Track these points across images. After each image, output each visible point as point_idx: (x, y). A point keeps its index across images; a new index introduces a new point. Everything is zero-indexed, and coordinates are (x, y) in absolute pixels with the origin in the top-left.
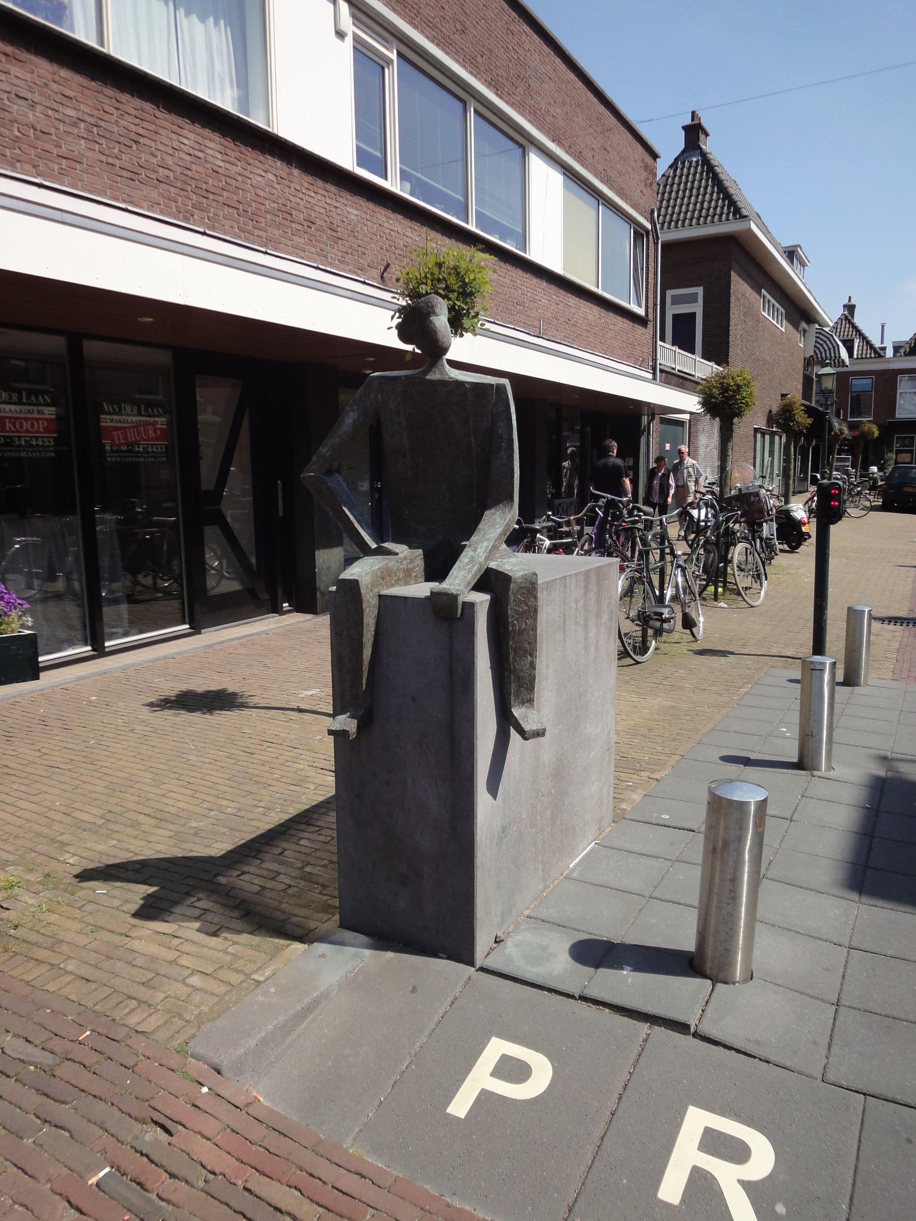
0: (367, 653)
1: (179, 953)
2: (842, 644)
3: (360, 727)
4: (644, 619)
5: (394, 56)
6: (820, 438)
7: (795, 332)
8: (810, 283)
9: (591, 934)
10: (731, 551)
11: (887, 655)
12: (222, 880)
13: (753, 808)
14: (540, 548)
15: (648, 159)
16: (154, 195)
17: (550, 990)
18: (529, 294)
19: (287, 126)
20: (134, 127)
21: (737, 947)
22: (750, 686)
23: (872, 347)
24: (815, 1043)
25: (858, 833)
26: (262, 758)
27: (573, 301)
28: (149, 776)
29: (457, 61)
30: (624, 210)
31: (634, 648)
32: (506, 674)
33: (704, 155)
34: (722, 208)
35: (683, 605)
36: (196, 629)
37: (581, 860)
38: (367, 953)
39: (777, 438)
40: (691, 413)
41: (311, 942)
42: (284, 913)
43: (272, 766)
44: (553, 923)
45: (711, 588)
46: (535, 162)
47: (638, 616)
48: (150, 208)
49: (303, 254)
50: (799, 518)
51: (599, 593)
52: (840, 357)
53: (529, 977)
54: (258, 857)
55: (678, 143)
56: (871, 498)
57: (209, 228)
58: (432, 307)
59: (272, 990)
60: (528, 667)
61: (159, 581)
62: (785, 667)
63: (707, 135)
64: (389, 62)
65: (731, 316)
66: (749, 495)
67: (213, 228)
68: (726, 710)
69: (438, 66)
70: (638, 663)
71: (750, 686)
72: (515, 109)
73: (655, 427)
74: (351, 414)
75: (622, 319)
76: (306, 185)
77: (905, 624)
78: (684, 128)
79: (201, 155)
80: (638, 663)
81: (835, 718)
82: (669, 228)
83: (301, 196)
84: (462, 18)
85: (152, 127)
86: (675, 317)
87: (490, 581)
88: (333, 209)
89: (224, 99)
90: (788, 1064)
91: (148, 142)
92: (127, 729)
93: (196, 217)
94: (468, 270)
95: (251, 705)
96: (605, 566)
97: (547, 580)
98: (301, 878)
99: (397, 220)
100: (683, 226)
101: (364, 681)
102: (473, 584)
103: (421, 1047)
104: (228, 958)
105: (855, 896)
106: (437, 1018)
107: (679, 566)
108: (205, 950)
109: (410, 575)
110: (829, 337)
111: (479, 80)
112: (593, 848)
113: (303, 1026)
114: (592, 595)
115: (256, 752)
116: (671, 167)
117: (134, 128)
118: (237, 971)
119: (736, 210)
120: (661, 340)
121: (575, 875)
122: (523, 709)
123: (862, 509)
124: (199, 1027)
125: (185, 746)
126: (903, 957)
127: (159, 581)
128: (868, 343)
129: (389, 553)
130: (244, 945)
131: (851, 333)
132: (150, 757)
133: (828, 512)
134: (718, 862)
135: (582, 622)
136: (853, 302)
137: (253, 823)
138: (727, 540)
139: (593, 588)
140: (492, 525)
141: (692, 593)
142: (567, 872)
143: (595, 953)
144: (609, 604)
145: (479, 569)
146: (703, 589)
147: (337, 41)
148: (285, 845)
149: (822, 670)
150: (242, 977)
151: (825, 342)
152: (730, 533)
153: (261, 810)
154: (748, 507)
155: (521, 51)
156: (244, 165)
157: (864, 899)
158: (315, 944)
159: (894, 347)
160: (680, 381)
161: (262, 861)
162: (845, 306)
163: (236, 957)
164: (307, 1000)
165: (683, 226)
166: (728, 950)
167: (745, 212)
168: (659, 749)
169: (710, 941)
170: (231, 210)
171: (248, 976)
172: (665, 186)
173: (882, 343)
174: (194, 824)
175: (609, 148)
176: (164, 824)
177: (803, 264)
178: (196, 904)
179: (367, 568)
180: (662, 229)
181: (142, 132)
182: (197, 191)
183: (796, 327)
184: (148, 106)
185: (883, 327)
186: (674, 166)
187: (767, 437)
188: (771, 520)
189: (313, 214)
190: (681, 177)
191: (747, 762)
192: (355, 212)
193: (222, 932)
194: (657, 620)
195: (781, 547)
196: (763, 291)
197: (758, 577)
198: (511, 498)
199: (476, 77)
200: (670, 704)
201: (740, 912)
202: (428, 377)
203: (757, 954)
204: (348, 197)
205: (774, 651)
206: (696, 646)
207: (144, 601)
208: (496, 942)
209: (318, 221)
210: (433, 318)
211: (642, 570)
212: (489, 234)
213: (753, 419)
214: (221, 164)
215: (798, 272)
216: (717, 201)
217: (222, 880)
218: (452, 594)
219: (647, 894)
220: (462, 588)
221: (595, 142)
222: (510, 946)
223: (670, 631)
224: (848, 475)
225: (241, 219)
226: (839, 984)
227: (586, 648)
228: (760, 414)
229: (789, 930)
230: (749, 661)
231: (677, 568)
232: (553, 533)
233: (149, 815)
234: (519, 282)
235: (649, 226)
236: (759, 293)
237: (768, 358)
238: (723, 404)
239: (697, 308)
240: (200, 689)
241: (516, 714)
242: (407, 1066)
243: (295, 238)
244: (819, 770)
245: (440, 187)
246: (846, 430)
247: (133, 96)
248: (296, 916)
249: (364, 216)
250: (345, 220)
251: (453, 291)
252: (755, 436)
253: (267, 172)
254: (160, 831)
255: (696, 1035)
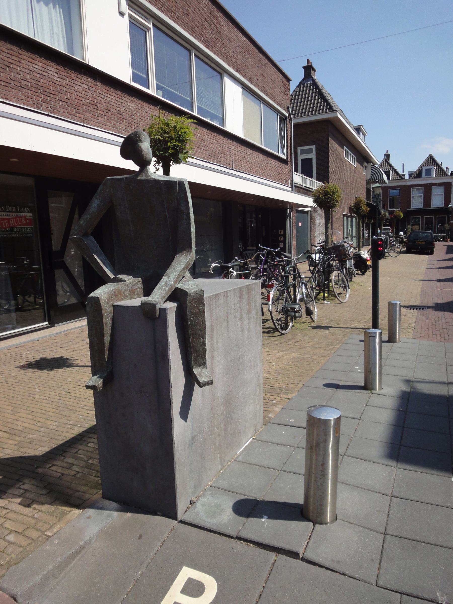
0: (107, 339)
1: (4, 519)
2: (387, 321)
3: (104, 384)
4: (285, 311)
5: (151, 26)
6: (375, 219)
7: (361, 167)
8: (368, 143)
9: (246, 495)
10: (331, 275)
11: (410, 326)
12: (40, 470)
13: (332, 422)
14: (231, 276)
15: (285, 81)
16: (20, 95)
17: (220, 534)
18: (226, 148)
19: (93, 60)
20: (7, 59)
21: (327, 503)
22: (340, 344)
23: (398, 174)
24: (372, 560)
25: (394, 425)
26: (75, 395)
27: (250, 152)
28: (11, 408)
29: (185, 30)
30: (274, 106)
31: (281, 325)
32: (189, 349)
33: (314, 81)
34: (323, 106)
35: (306, 303)
36: (52, 324)
37: (244, 449)
38: (116, 514)
39: (354, 219)
40: (311, 207)
41: (84, 508)
42: (72, 489)
43: (80, 400)
44: (225, 490)
45: (322, 294)
46: (227, 82)
47: (282, 310)
48: (18, 101)
49: (104, 127)
50: (365, 257)
51: (249, 300)
52: (383, 179)
53: (208, 526)
54: (63, 455)
55: (301, 75)
56: (401, 247)
57: (51, 113)
58: (139, 137)
59: (56, 541)
60: (201, 344)
61: (37, 300)
62: (359, 334)
63: (315, 71)
64: (149, 29)
65: (330, 159)
66: (339, 246)
67: (54, 113)
68: (328, 358)
69: (178, 34)
70: (283, 334)
71: (340, 344)
72: (216, 55)
73: (293, 214)
74: (96, 201)
75: (275, 161)
76: (105, 91)
77: (418, 309)
78: (304, 67)
79: (45, 74)
80: (283, 334)
81: (383, 361)
82: (298, 116)
83: (103, 96)
84: (186, 8)
85: (18, 59)
86: (302, 160)
87: (176, 295)
88: (120, 104)
89: (60, 46)
90: (356, 576)
91: (15, 67)
92: (4, 381)
93: (44, 107)
94: (181, 128)
95: (75, 365)
96: (252, 284)
97: (215, 293)
98: (85, 467)
99: (155, 110)
100: (305, 115)
101: (106, 356)
102: (167, 297)
103: (141, 575)
104: (33, 521)
105: (394, 463)
106: (155, 552)
107: (303, 283)
108: (21, 517)
109: (134, 293)
110: (378, 169)
111: (197, 39)
112: (251, 442)
113: (73, 564)
114: (245, 301)
115: (73, 392)
116: (298, 87)
117: (7, 59)
118: (37, 530)
119: (330, 107)
120: (295, 171)
121: (240, 459)
122: (200, 369)
123: (396, 253)
124: (8, 569)
125: (34, 390)
126: (422, 501)
127: (37, 300)
128: (397, 172)
129: (121, 281)
130: (44, 512)
131: (388, 167)
132: (13, 397)
133: (377, 255)
134: (314, 455)
135: (239, 316)
136: (389, 153)
137: (64, 434)
138: (328, 270)
139: (245, 297)
140: (179, 263)
141: (310, 297)
142: (236, 457)
143: (247, 508)
144: (256, 305)
145: (170, 289)
146: (318, 294)
147: (120, 17)
148: (81, 447)
149: (375, 337)
150: (40, 533)
151: (376, 172)
152: (330, 266)
153: (70, 426)
154: (336, 252)
155: (218, 26)
156: (70, 80)
157: (400, 465)
158: (86, 509)
159: (409, 174)
160: (305, 191)
161: (65, 457)
162: (385, 155)
163: (38, 520)
164: (75, 548)
165: (305, 115)
166: (321, 505)
167: (334, 108)
168: (291, 381)
169: (312, 499)
170: (63, 103)
171: (43, 532)
172: (295, 96)
173: (403, 172)
174: (30, 436)
175: (265, 76)
176: (14, 437)
177: (364, 134)
178: (22, 487)
179: (106, 290)
180: (294, 117)
181: (11, 61)
182: (44, 93)
183: (362, 164)
184: (15, 48)
185: (403, 164)
186: (299, 86)
187: (349, 219)
188: (351, 259)
189: (109, 106)
190: (303, 91)
191: (337, 387)
192: (132, 105)
193: (33, 504)
194: (292, 311)
195: (357, 272)
196: (345, 147)
197: (345, 288)
198: (190, 247)
199: (195, 38)
200: (299, 355)
201: (328, 483)
202: (138, 178)
203: (339, 503)
204: (128, 97)
205: (353, 326)
206: (313, 324)
207: (30, 310)
208: (191, 504)
209: (112, 110)
210: (140, 144)
211: (284, 286)
212: (205, 118)
213: (341, 209)
214: (57, 79)
215: (362, 138)
216: (321, 103)
217: (40, 470)
218: (153, 304)
219: (279, 469)
220: (159, 300)
221: (258, 72)
222: (199, 506)
223: (299, 317)
224: (389, 236)
225: (69, 108)
226: (385, 520)
227: (242, 331)
228: (345, 208)
229: (358, 487)
230: (340, 331)
231: (302, 284)
232: (242, 267)
233: (6, 432)
234: (220, 141)
235: (287, 114)
236: (343, 148)
237: (348, 180)
238: (325, 201)
239: (313, 156)
240: (49, 357)
241: (195, 372)
242: (132, 588)
243: (100, 118)
244: (375, 390)
245: (178, 93)
246: (387, 215)
247: (6, 42)
248: (78, 491)
249: (137, 107)
250: (127, 109)
251: (174, 139)
252: (343, 219)
253: (83, 84)
254: (11, 442)
255: (303, 559)
